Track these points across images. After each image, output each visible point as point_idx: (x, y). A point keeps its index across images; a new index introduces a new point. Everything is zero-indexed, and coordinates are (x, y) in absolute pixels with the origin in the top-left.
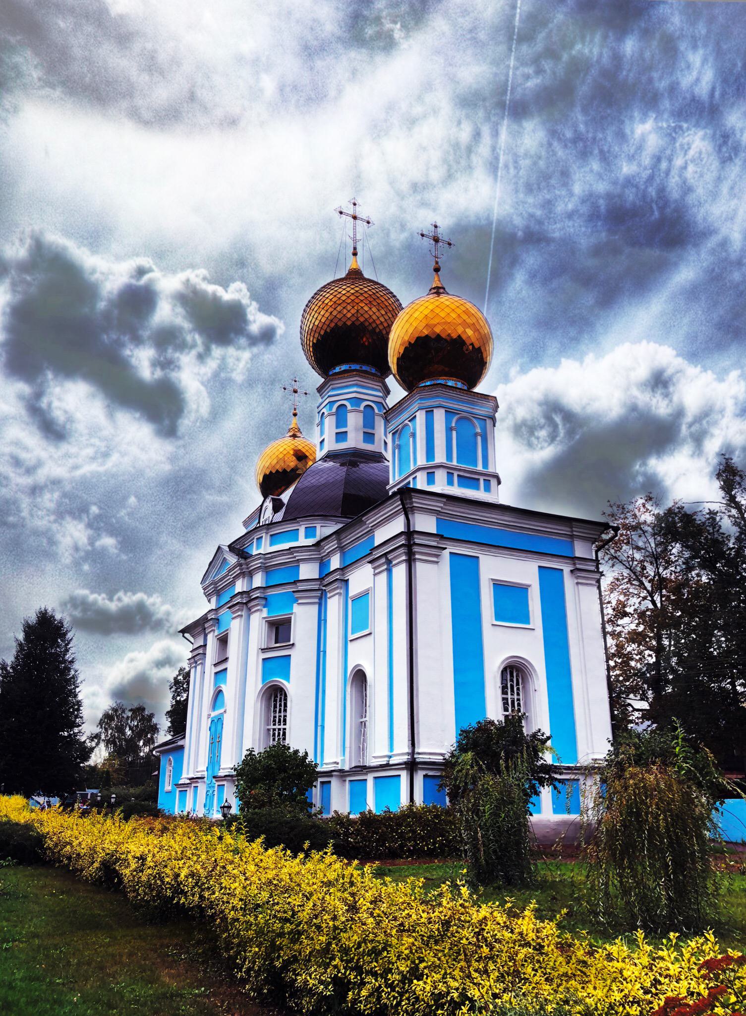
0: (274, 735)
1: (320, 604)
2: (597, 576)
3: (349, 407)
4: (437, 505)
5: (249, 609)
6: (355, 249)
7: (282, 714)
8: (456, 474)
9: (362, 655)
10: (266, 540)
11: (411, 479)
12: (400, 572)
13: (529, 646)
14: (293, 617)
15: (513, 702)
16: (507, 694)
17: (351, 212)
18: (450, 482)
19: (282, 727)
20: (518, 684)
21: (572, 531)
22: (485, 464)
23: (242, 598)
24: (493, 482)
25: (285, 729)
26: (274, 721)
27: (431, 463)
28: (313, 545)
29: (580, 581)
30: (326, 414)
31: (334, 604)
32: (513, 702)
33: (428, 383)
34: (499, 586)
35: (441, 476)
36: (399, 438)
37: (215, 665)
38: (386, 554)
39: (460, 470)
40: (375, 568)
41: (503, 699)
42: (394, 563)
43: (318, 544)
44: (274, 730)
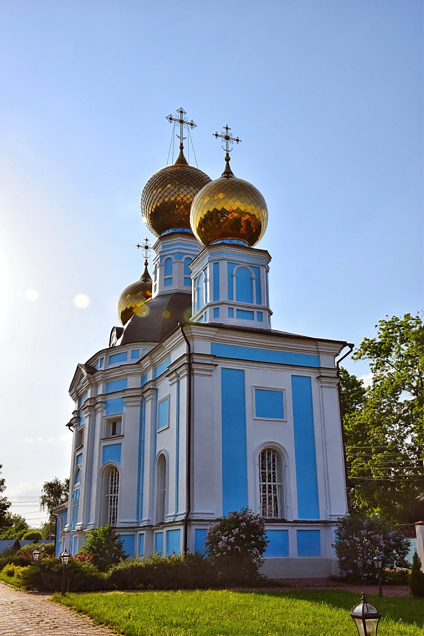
0: (111, 500)
1: (142, 406)
3: (174, 260)
4: (212, 332)
6: (182, 144)
8: (235, 308)
12: (184, 382)
13: (283, 435)
14: (123, 415)
15: (269, 475)
18: (231, 315)
21: (318, 349)
22: (259, 301)
24: (266, 313)
26: (275, 489)
27: (216, 302)
28: (136, 364)
29: (323, 385)
32: (269, 475)
35: (224, 310)
38: (176, 370)
39: (239, 306)
43: (138, 363)
44: (111, 497)
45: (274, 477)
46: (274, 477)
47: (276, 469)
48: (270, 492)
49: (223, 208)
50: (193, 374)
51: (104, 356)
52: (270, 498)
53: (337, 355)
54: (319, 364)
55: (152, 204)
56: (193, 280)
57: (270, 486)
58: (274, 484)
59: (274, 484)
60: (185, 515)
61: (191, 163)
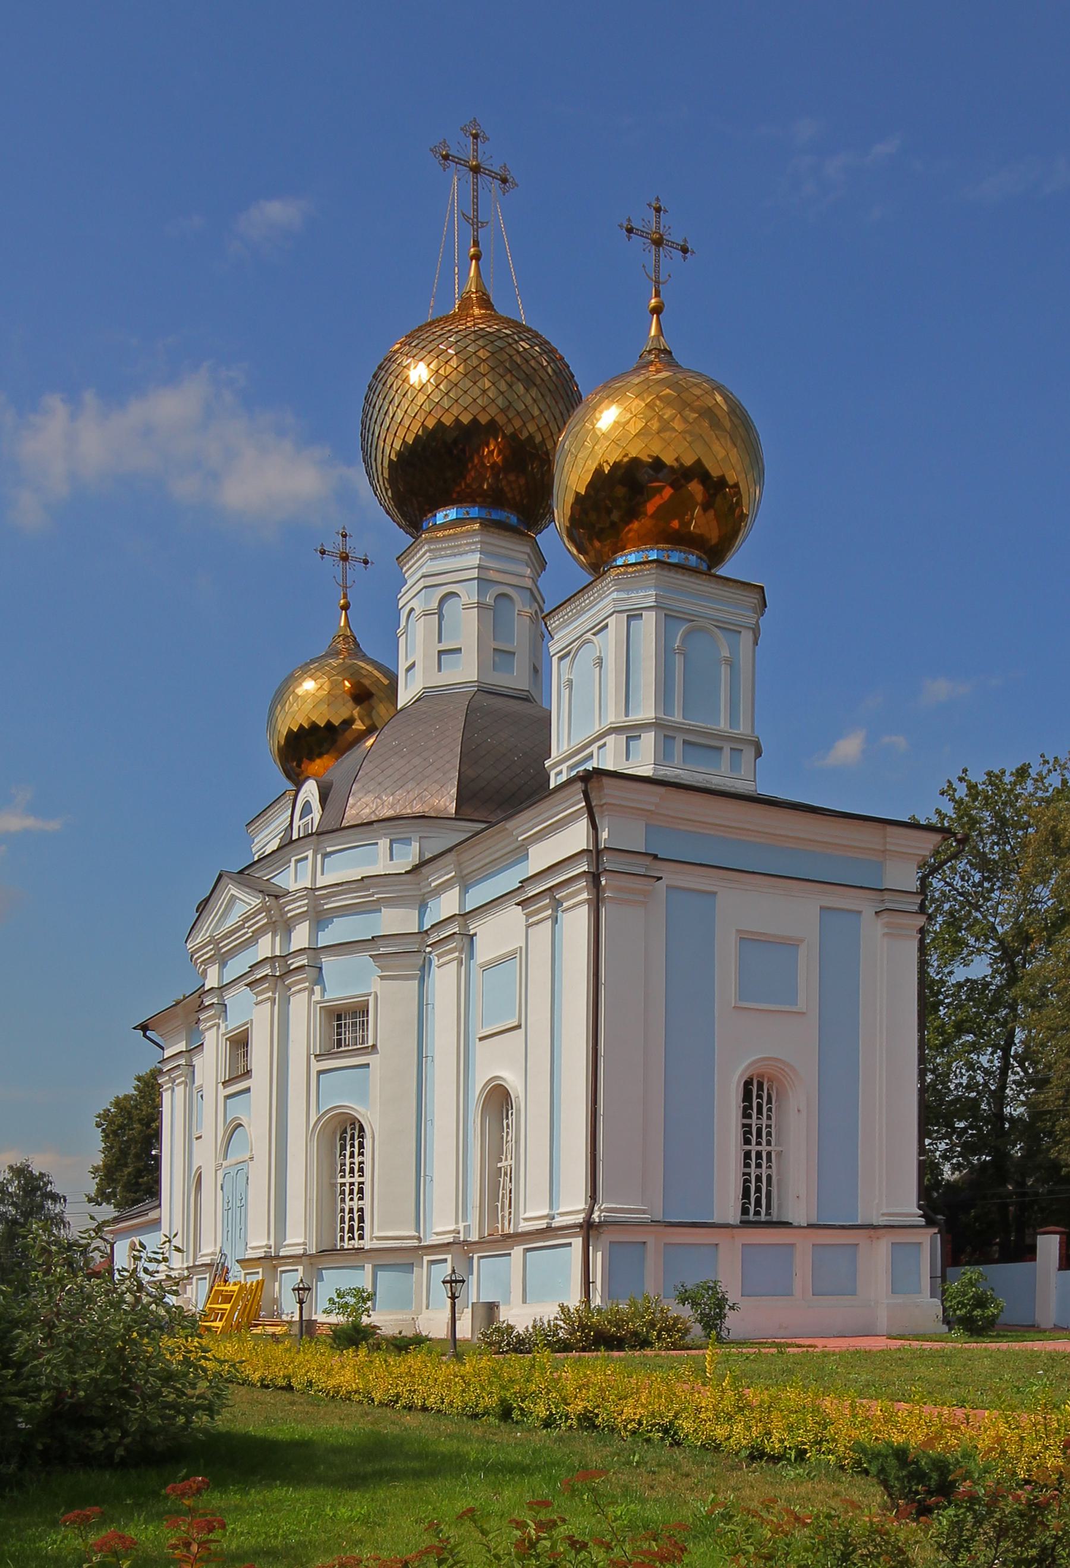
4: (652, 796)
7: (356, 1160)
9: (498, 1063)
11: (594, 748)
14: (371, 999)
16: (750, 1116)
20: (769, 1101)
23: (273, 968)
26: (769, 1160)
28: (407, 873)
30: (417, 611)
31: (444, 978)
33: (632, 559)
34: (747, 940)
36: (571, 666)
37: (225, 1084)
40: (528, 916)
41: (744, 1126)
42: (565, 905)
45: (769, 1134)
46: (769, 1134)
47: (773, 1118)
48: (759, 1166)
49: (699, 462)
51: (310, 853)
52: (759, 1179)
55: (394, 426)
56: (555, 659)
57: (759, 1155)
58: (769, 1148)
59: (769, 1148)
60: (583, 1215)
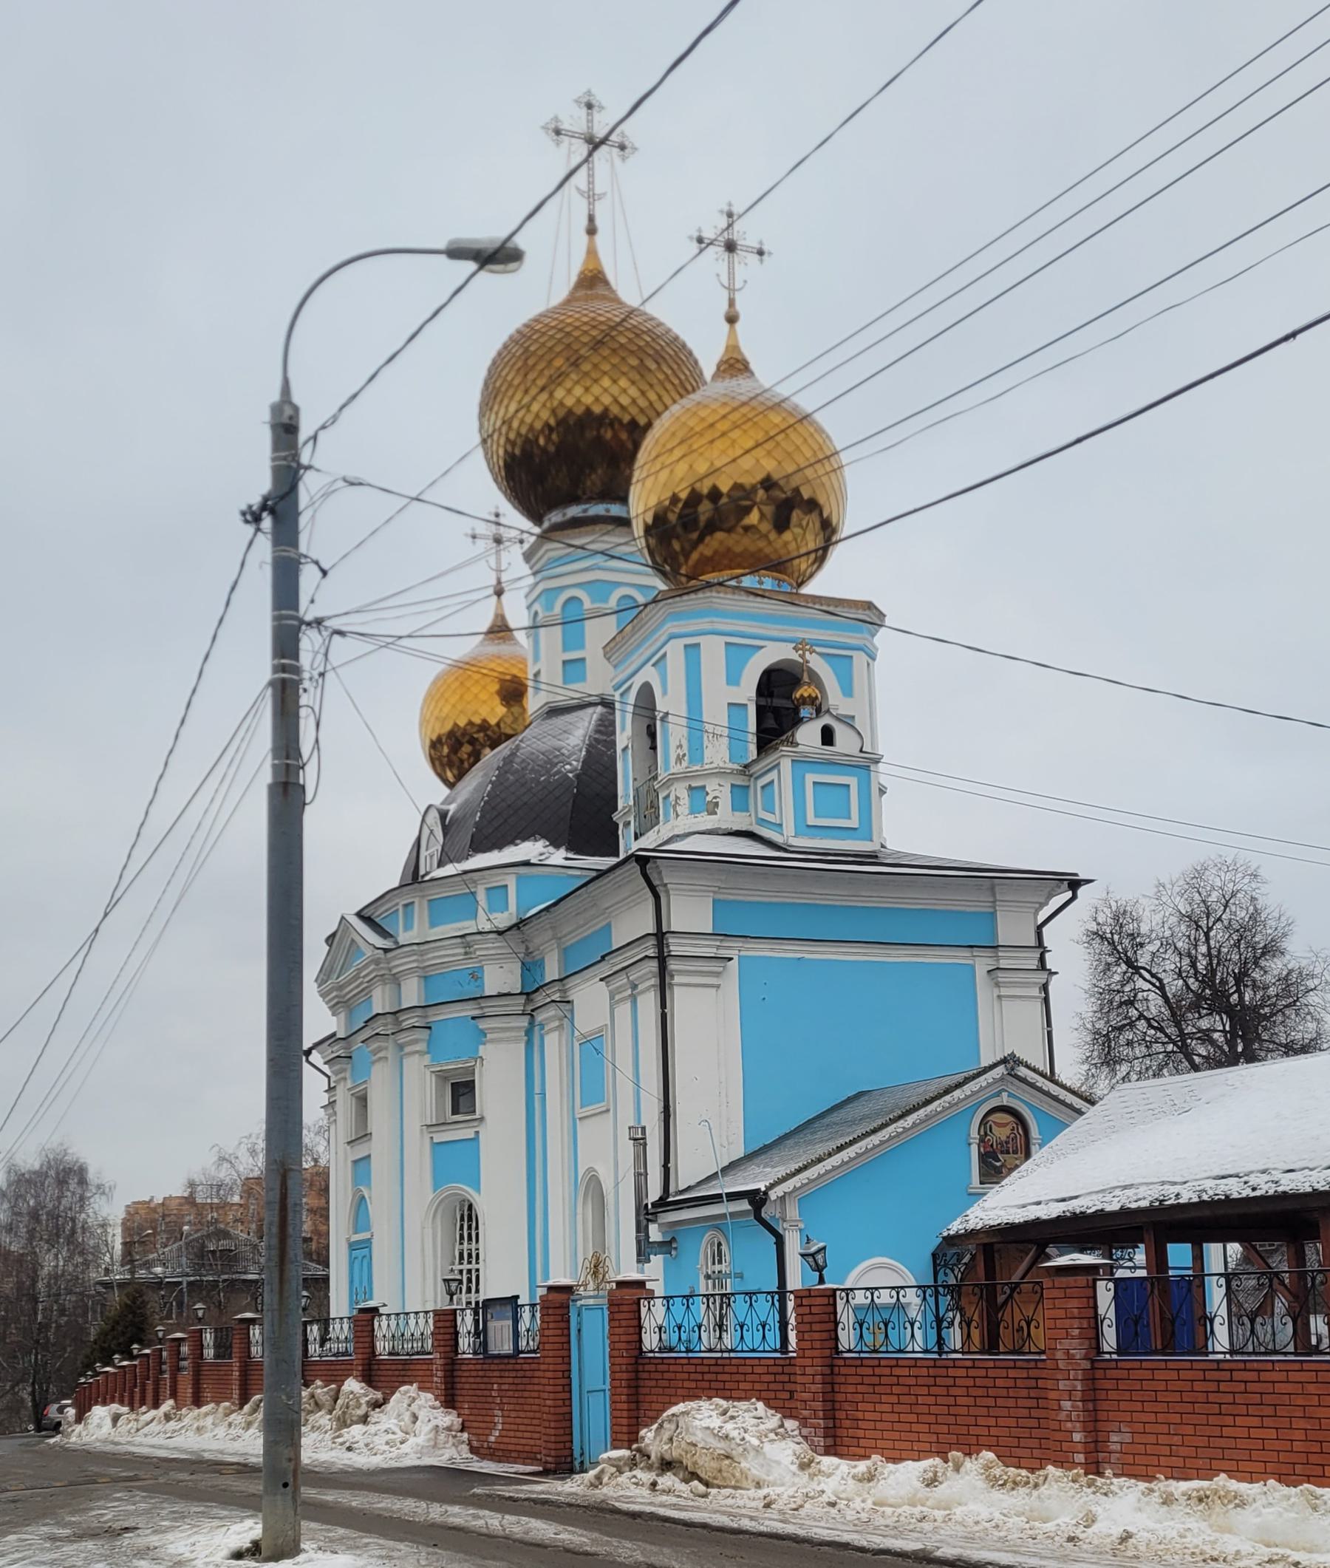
1: (529, 1044)
2: (1042, 977)
5: (401, 1047)
6: (591, 219)
10: (420, 912)
12: (649, 1002)
17: (581, 127)
19: (473, 1266)
25: (477, 1270)
29: (1004, 991)
50: (671, 985)
53: (1042, 905)
54: (995, 934)
61: (628, 290)
